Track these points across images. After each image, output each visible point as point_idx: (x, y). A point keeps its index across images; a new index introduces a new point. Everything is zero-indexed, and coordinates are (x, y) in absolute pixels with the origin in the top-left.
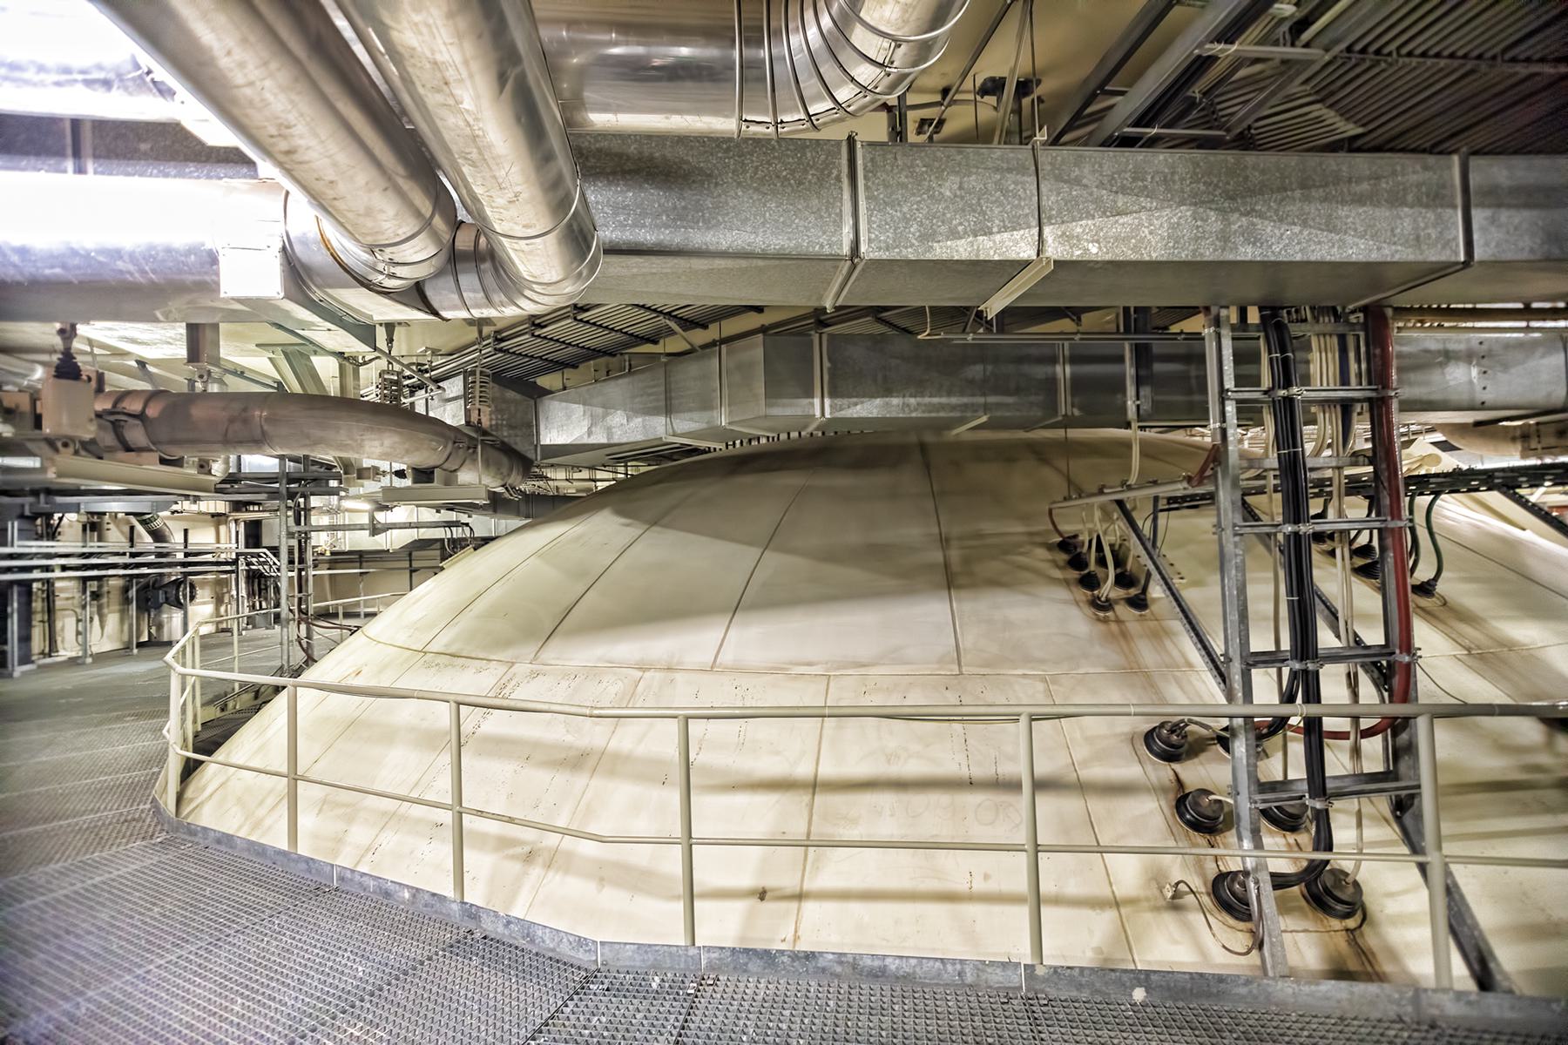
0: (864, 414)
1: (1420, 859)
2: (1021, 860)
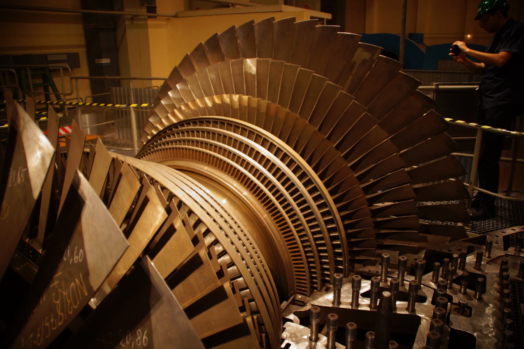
0: (356, 174)
1: (25, 106)
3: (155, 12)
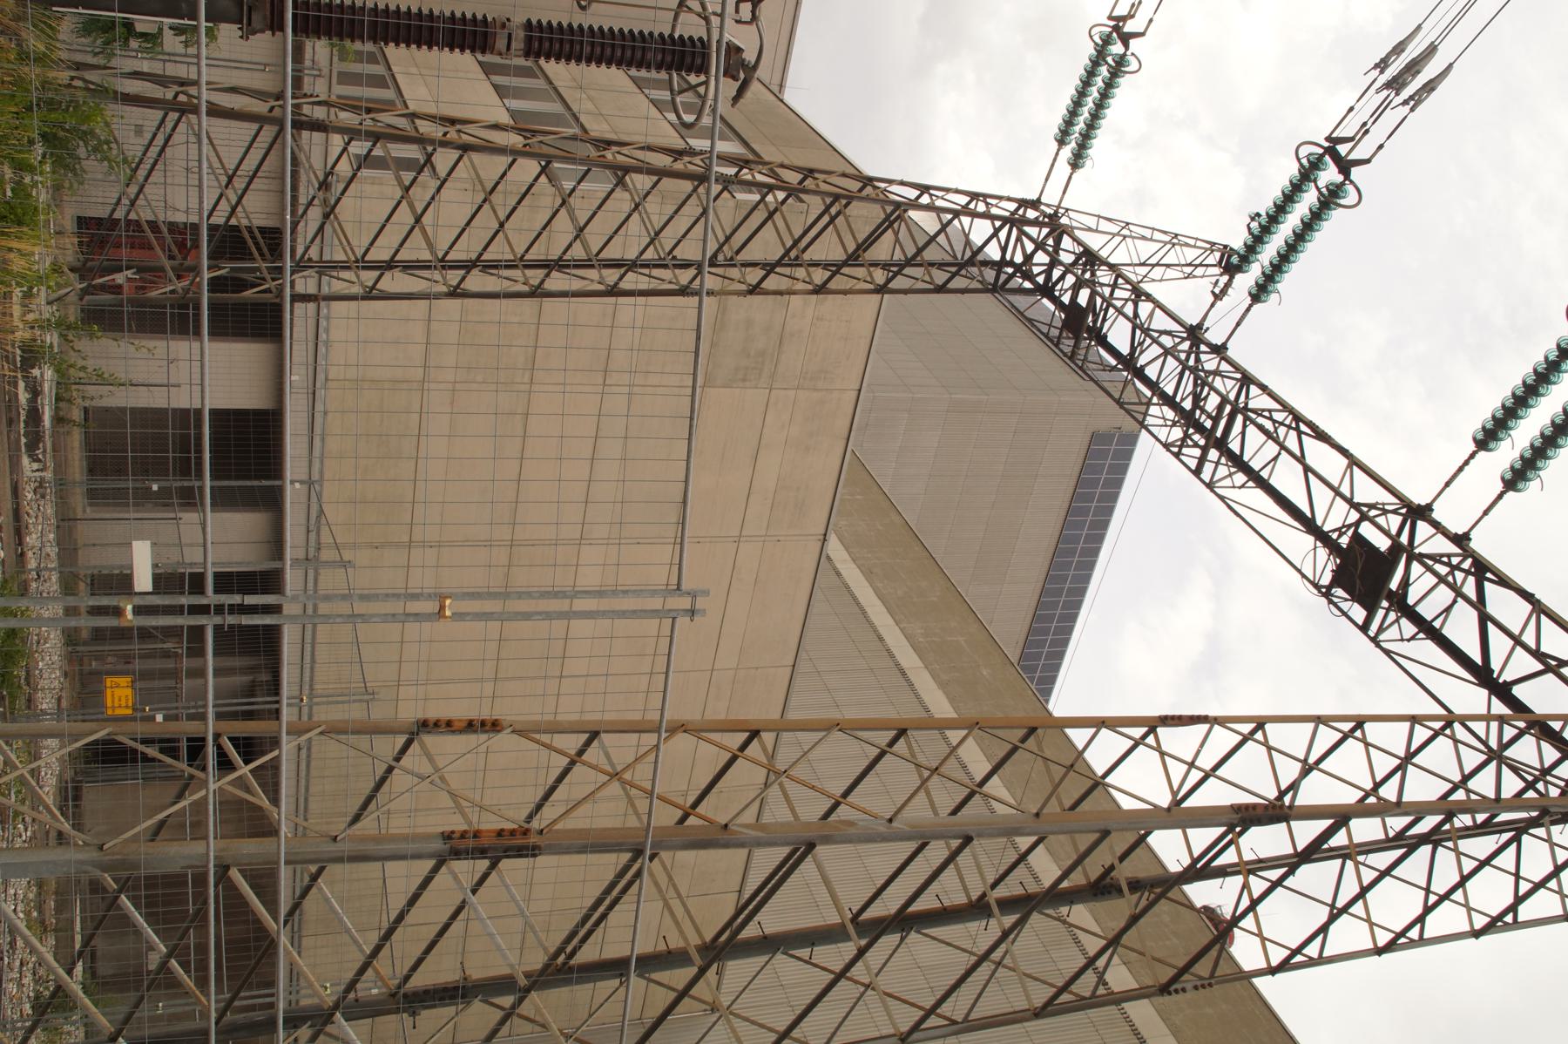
2: (1150, 412)
3: (167, 409)
